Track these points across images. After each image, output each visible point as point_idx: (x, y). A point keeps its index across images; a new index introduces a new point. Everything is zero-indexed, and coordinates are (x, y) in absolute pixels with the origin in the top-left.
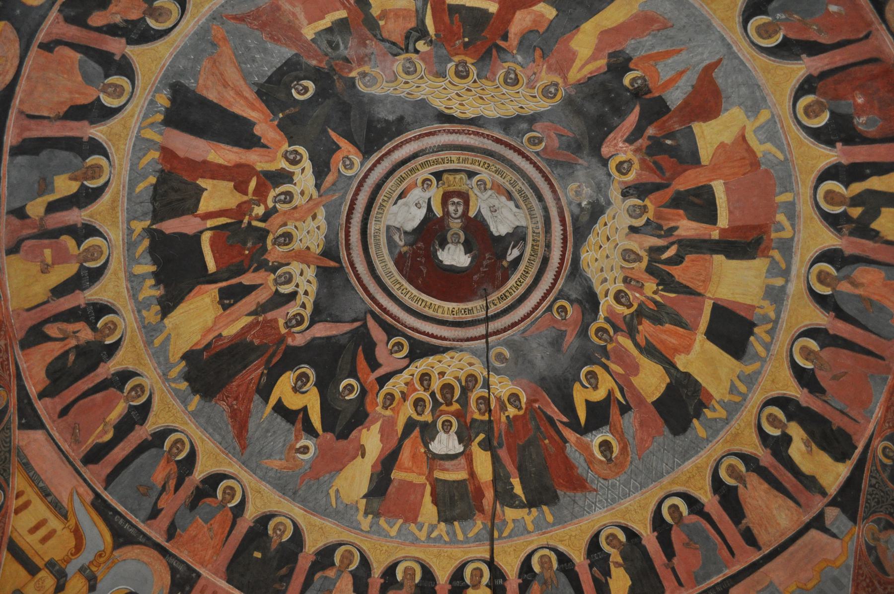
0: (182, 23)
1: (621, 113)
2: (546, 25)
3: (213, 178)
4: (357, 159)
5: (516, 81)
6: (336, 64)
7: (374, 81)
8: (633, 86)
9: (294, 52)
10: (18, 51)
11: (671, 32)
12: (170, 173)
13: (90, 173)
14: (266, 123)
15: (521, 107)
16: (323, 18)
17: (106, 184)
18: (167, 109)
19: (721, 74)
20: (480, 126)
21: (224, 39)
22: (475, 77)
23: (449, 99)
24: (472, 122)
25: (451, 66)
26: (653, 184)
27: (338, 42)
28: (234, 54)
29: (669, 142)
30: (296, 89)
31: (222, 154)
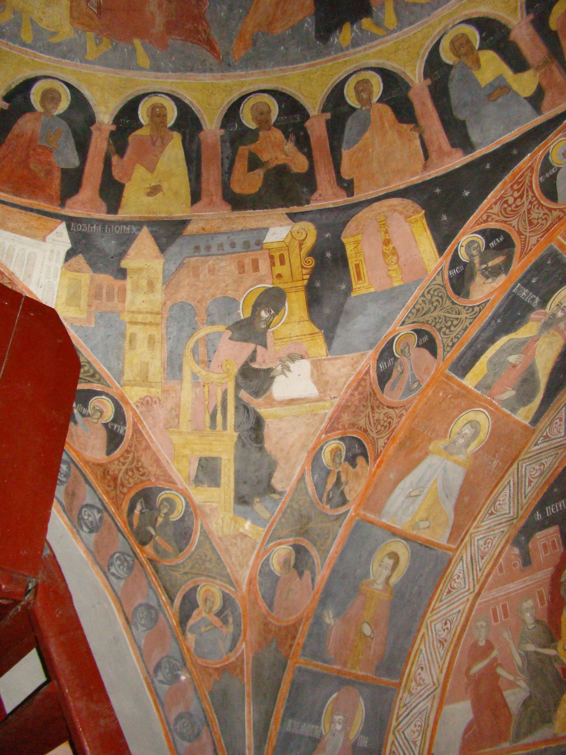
10: (365, 210)
13: (463, 50)
17: (469, 21)
18: (352, 24)
28: (248, 13)
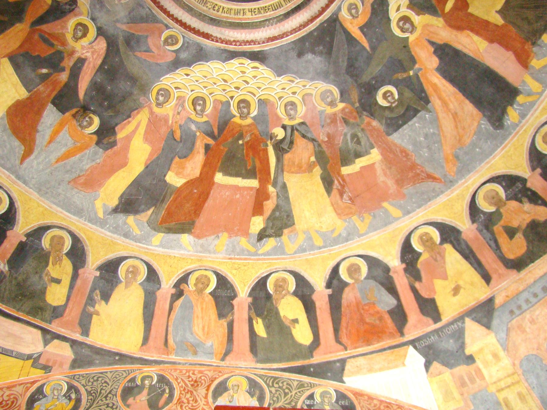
0: (478, 184)
1: (96, 87)
2: (173, 165)
3: (487, 23)
4: (344, 14)
5: (194, 102)
6: (355, 118)
7: (323, 96)
8: (90, 118)
9: (391, 138)
11: (68, 177)
12: (527, 39)
14: (426, 68)
15: (187, 75)
16: (361, 168)
19: (17, 150)
20: (225, 51)
21: (446, 159)
22: (232, 103)
23: (255, 77)
24: (233, 55)
25: (254, 112)
26: (47, 22)
27: (351, 142)
29: (45, 71)
30: (393, 98)
31: (472, 45)
